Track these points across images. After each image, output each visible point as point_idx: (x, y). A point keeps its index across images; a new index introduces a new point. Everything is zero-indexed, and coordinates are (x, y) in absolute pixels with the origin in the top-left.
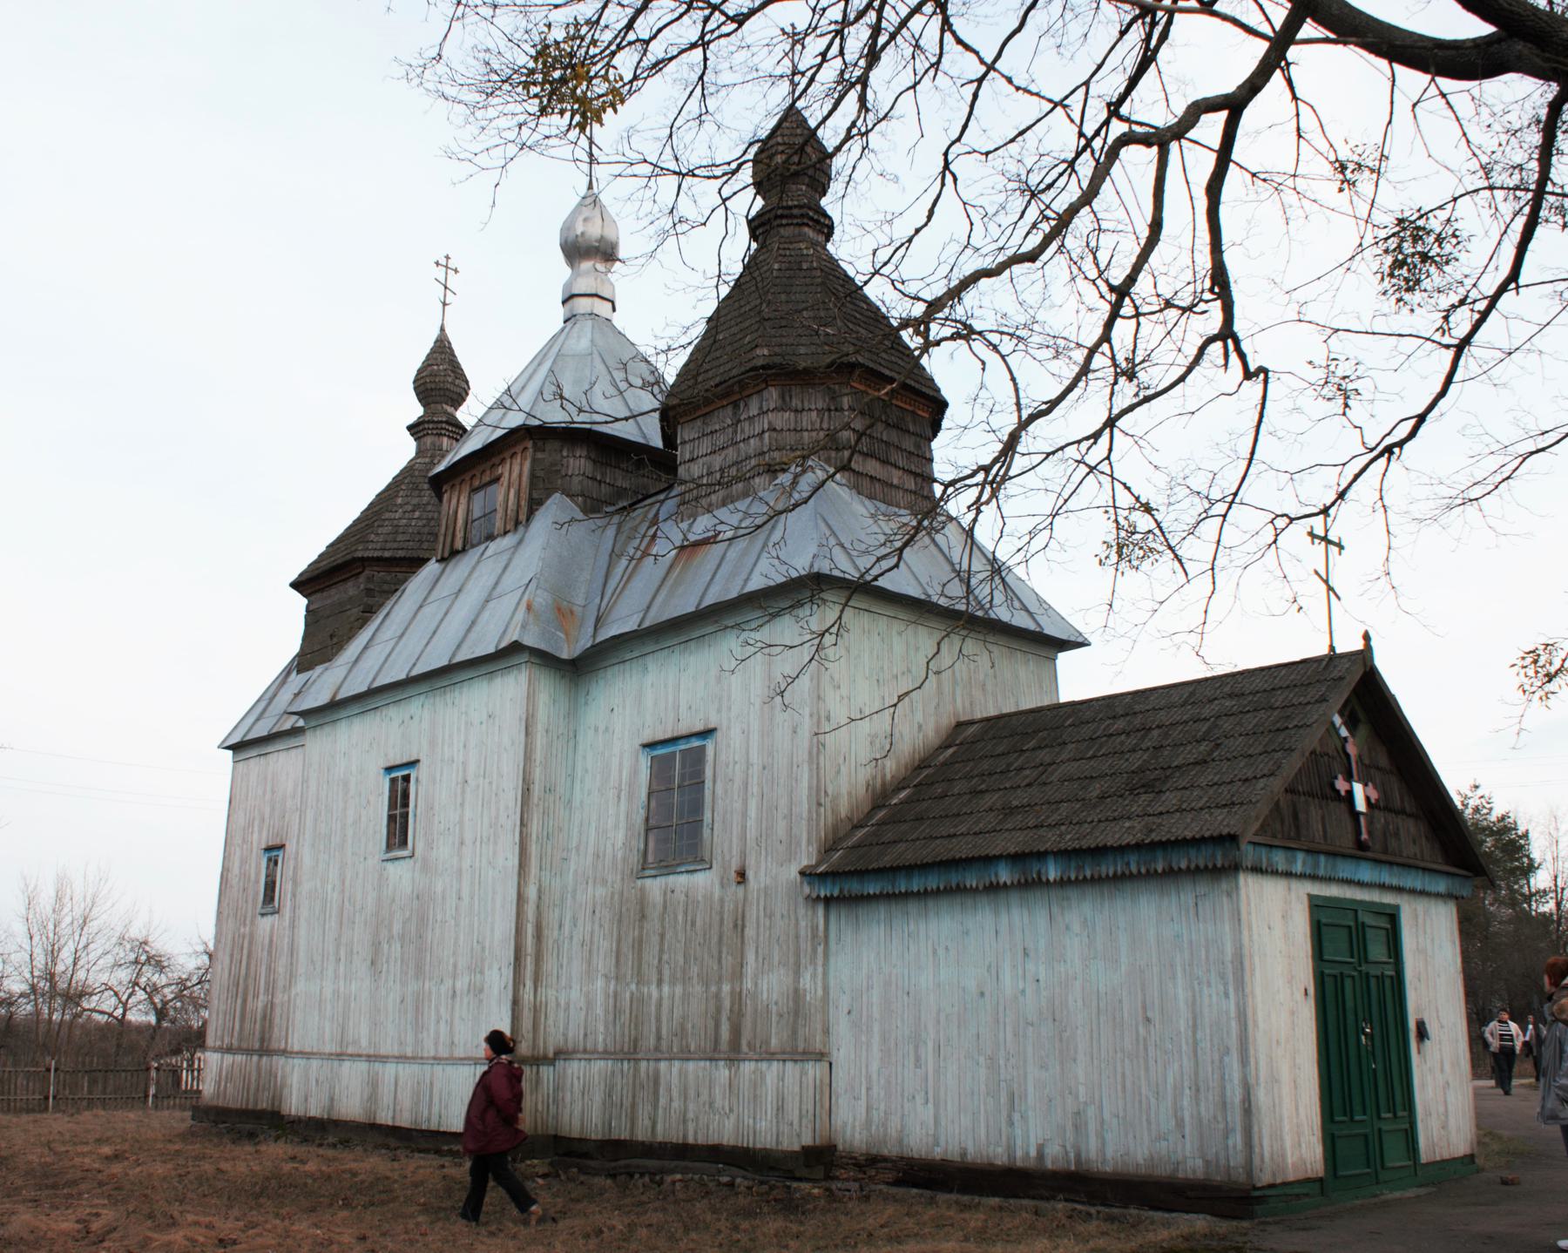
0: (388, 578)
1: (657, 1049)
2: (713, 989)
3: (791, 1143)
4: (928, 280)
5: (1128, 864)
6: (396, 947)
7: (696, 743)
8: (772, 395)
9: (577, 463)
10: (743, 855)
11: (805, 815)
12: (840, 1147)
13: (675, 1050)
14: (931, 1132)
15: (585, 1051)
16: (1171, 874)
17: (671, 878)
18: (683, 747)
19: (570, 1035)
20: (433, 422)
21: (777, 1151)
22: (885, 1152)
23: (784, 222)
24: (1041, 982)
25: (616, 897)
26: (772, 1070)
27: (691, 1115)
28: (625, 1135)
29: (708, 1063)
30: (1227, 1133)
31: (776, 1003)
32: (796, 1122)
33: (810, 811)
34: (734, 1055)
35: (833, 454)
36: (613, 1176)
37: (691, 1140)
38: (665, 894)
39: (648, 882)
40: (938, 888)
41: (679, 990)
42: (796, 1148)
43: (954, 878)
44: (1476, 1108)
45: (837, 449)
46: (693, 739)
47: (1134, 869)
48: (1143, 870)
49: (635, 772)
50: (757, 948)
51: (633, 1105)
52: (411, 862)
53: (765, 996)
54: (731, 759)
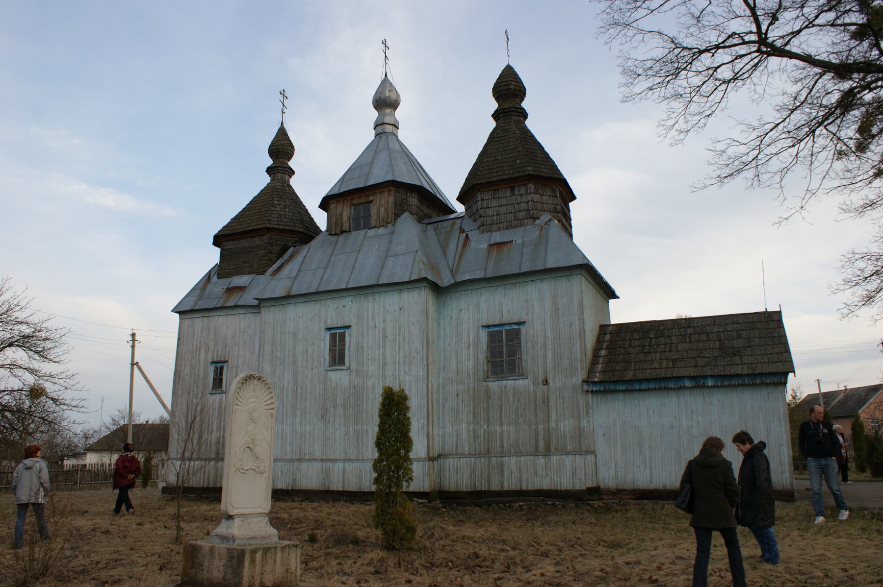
0: (280, 238)
1: (501, 452)
2: (533, 427)
3: (579, 486)
4: (788, 168)
5: (744, 381)
6: (340, 411)
7: (515, 327)
8: (531, 187)
9: (414, 200)
10: (545, 373)
11: (579, 358)
12: (602, 487)
13: (512, 452)
14: (648, 479)
15: (457, 454)
16: (762, 384)
17: (504, 382)
18: (507, 328)
19: (446, 448)
20: (283, 167)
21: (573, 490)
22: (626, 488)
23: (514, 113)
24: (700, 423)
25: (471, 389)
26: (568, 459)
27: (524, 478)
28: (484, 488)
29: (532, 457)
30: (782, 473)
31: (569, 432)
32: (583, 477)
33: (581, 357)
34: (548, 452)
35: (555, 214)
36: (479, 506)
37: (524, 488)
38: (501, 388)
39: (490, 383)
40: (655, 388)
41: (512, 428)
42: (584, 488)
43: (663, 385)
44: (793, 463)
45: (557, 213)
46: (513, 325)
47: (747, 382)
48: (751, 383)
49: (478, 336)
50: (557, 411)
51: (489, 476)
52: (348, 372)
53: (562, 429)
54: (536, 335)
